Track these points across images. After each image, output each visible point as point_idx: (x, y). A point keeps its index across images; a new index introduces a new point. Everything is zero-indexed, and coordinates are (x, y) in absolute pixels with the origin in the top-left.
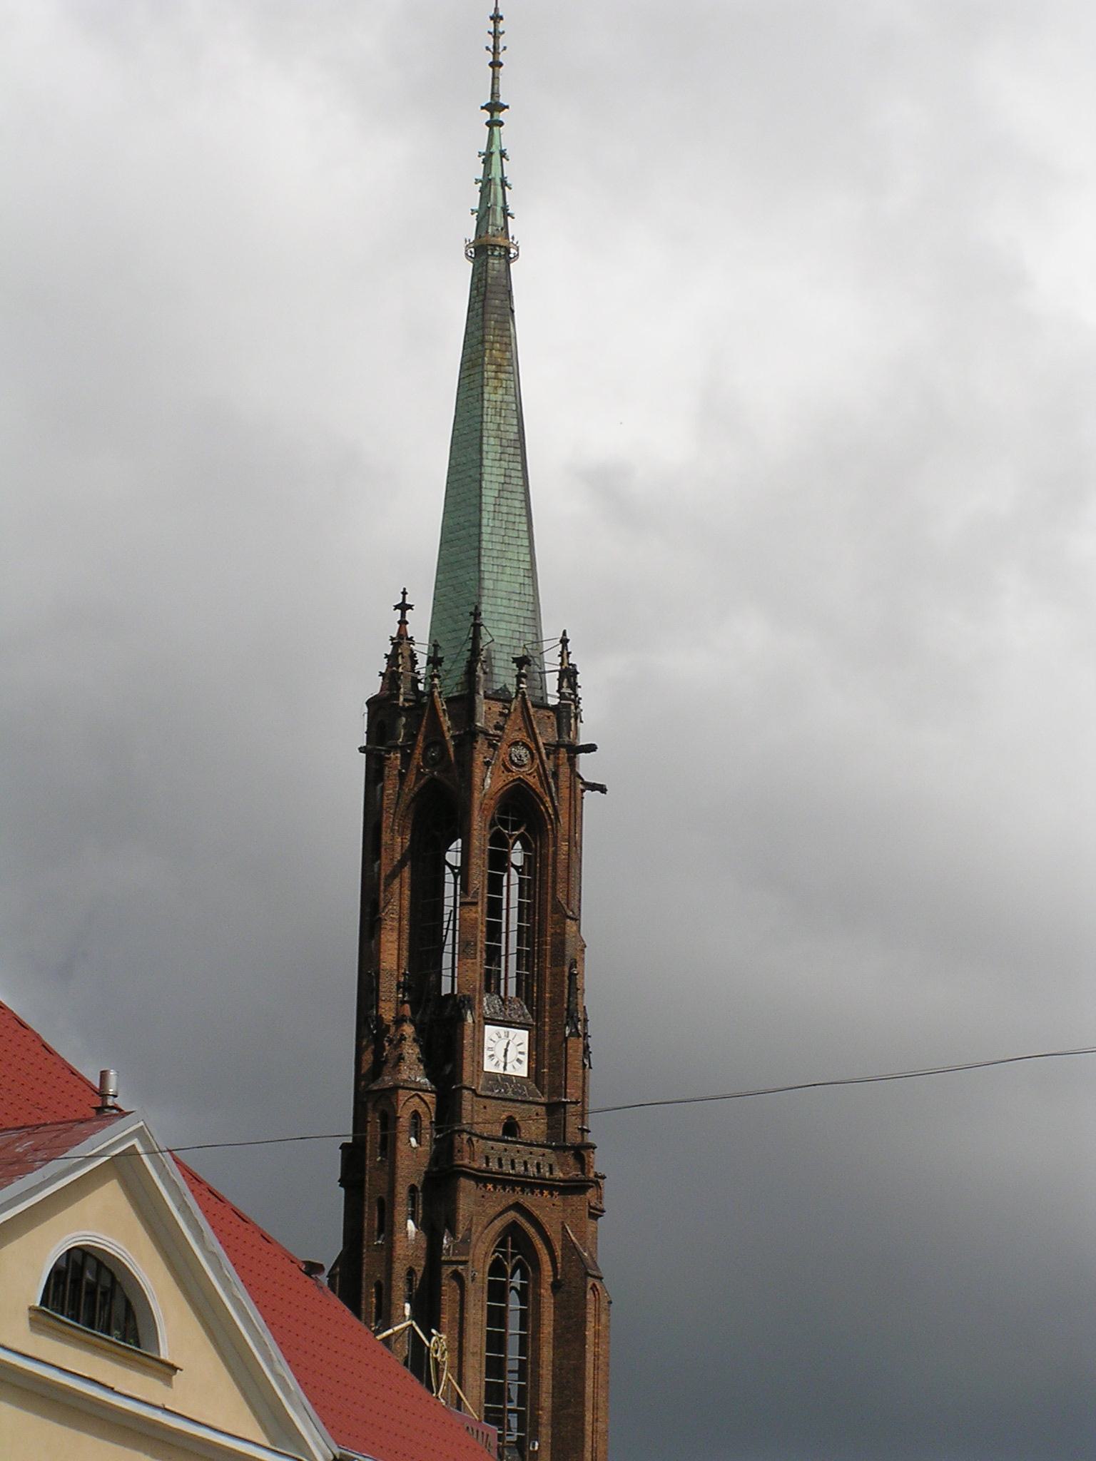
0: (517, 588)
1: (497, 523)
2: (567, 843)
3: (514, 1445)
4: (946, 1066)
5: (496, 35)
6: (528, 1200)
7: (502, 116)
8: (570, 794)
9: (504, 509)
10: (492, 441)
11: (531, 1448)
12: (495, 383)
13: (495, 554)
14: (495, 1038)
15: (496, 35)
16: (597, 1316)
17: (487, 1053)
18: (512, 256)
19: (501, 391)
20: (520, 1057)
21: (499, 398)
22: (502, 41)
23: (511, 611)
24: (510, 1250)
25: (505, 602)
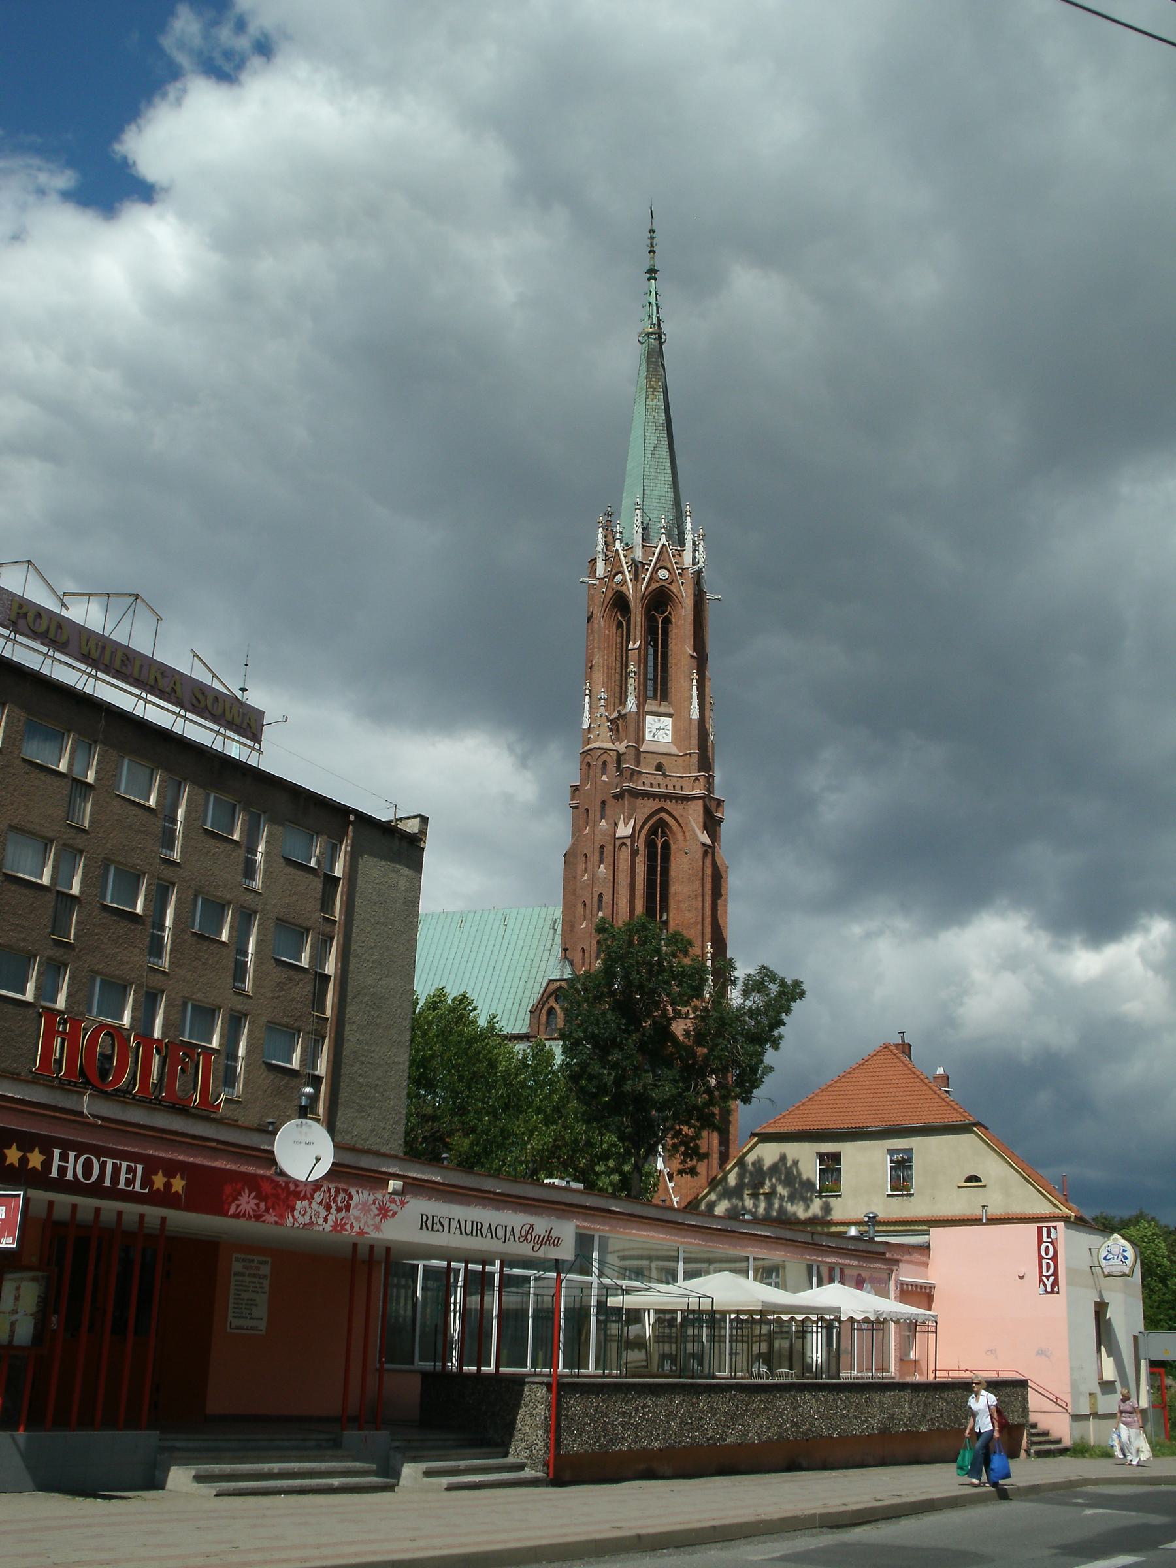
0: (664, 494)
1: (653, 463)
2: (57, 1152)
3: (526, 1380)
4: (619, 640)
5: (652, 238)
6: (668, 806)
7: (654, 235)
8: (279, 1025)
9: (657, 456)
10: (650, 424)
11: (235, 1256)
12: (653, 397)
13: (652, 478)
14: (653, 722)
15: (652, 238)
16: (734, 1351)
17: (647, 730)
18: (663, 340)
19: (655, 400)
20: (667, 732)
21: (654, 403)
22: (655, 242)
23: (661, 505)
24: (594, 1279)
25: (657, 501)
